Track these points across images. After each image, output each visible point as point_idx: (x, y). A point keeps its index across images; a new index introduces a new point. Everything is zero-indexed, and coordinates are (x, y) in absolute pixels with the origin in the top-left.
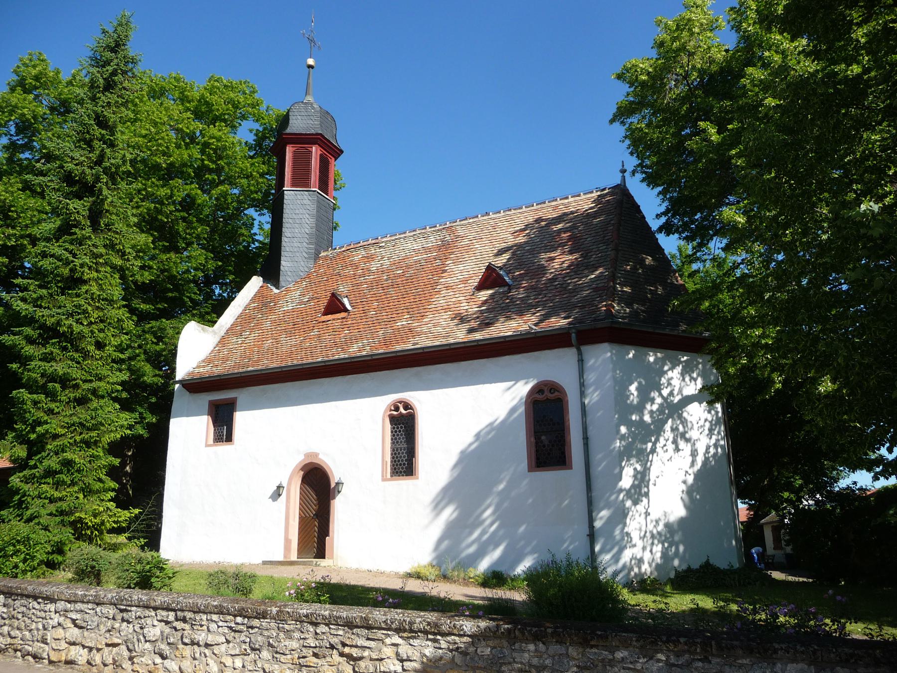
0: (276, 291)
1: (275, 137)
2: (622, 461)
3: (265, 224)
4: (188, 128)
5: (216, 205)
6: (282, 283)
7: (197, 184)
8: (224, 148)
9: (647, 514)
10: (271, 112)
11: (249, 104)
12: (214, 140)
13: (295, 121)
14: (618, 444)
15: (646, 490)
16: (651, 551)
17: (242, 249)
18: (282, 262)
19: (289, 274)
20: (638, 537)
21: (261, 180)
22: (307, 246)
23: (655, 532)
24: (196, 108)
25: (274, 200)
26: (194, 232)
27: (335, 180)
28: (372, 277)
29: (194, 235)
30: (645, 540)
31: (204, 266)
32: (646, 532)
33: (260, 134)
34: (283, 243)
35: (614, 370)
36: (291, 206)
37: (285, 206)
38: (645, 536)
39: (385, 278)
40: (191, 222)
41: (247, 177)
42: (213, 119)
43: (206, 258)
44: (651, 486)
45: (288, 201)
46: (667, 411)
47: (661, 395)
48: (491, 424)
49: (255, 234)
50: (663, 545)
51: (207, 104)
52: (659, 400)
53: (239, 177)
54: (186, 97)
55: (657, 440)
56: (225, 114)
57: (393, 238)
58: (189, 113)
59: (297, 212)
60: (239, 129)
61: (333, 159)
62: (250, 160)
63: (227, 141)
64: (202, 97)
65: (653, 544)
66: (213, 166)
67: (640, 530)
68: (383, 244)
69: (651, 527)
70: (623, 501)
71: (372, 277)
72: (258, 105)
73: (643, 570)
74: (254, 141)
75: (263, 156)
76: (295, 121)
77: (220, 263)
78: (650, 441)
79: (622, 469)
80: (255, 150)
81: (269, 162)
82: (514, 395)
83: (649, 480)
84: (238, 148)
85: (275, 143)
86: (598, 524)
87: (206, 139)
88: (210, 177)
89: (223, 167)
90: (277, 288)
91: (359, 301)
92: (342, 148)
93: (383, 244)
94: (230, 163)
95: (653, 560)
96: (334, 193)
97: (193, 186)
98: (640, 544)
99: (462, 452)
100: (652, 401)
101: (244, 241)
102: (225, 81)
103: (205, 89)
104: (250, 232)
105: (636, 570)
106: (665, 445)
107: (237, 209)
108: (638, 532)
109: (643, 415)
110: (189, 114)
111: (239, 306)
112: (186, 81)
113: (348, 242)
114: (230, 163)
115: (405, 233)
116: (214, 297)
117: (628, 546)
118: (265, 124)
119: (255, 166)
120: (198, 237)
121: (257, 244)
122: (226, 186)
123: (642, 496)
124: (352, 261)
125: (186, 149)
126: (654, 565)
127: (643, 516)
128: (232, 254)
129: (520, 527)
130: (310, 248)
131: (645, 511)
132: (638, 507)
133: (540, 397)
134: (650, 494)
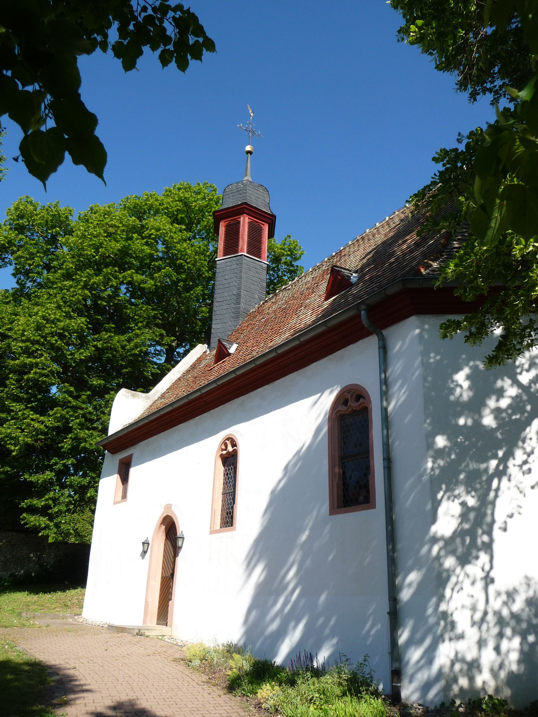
2: (438, 492)
9: (488, 580)
14: (430, 465)
15: (486, 538)
16: (497, 649)
20: (469, 622)
23: (505, 612)
30: (484, 627)
32: (486, 613)
35: (425, 354)
38: (483, 619)
44: (497, 533)
46: (529, 408)
47: (516, 382)
48: (299, 452)
50: (524, 638)
52: (512, 391)
55: (509, 454)
59: (227, 277)
65: (501, 635)
67: (474, 609)
69: (496, 604)
70: (438, 557)
73: (479, 681)
78: (495, 456)
79: (437, 504)
82: (318, 412)
83: (493, 521)
86: (405, 595)
95: (501, 666)
98: (473, 634)
99: (273, 492)
100: (500, 393)
105: (463, 682)
106: (525, 462)
108: (468, 613)
109: (481, 417)
117: (447, 636)
123: (479, 550)
126: (503, 674)
127: (480, 584)
129: (320, 595)
131: (483, 575)
132: (469, 568)
133: (342, 408)
134: (495, 546)
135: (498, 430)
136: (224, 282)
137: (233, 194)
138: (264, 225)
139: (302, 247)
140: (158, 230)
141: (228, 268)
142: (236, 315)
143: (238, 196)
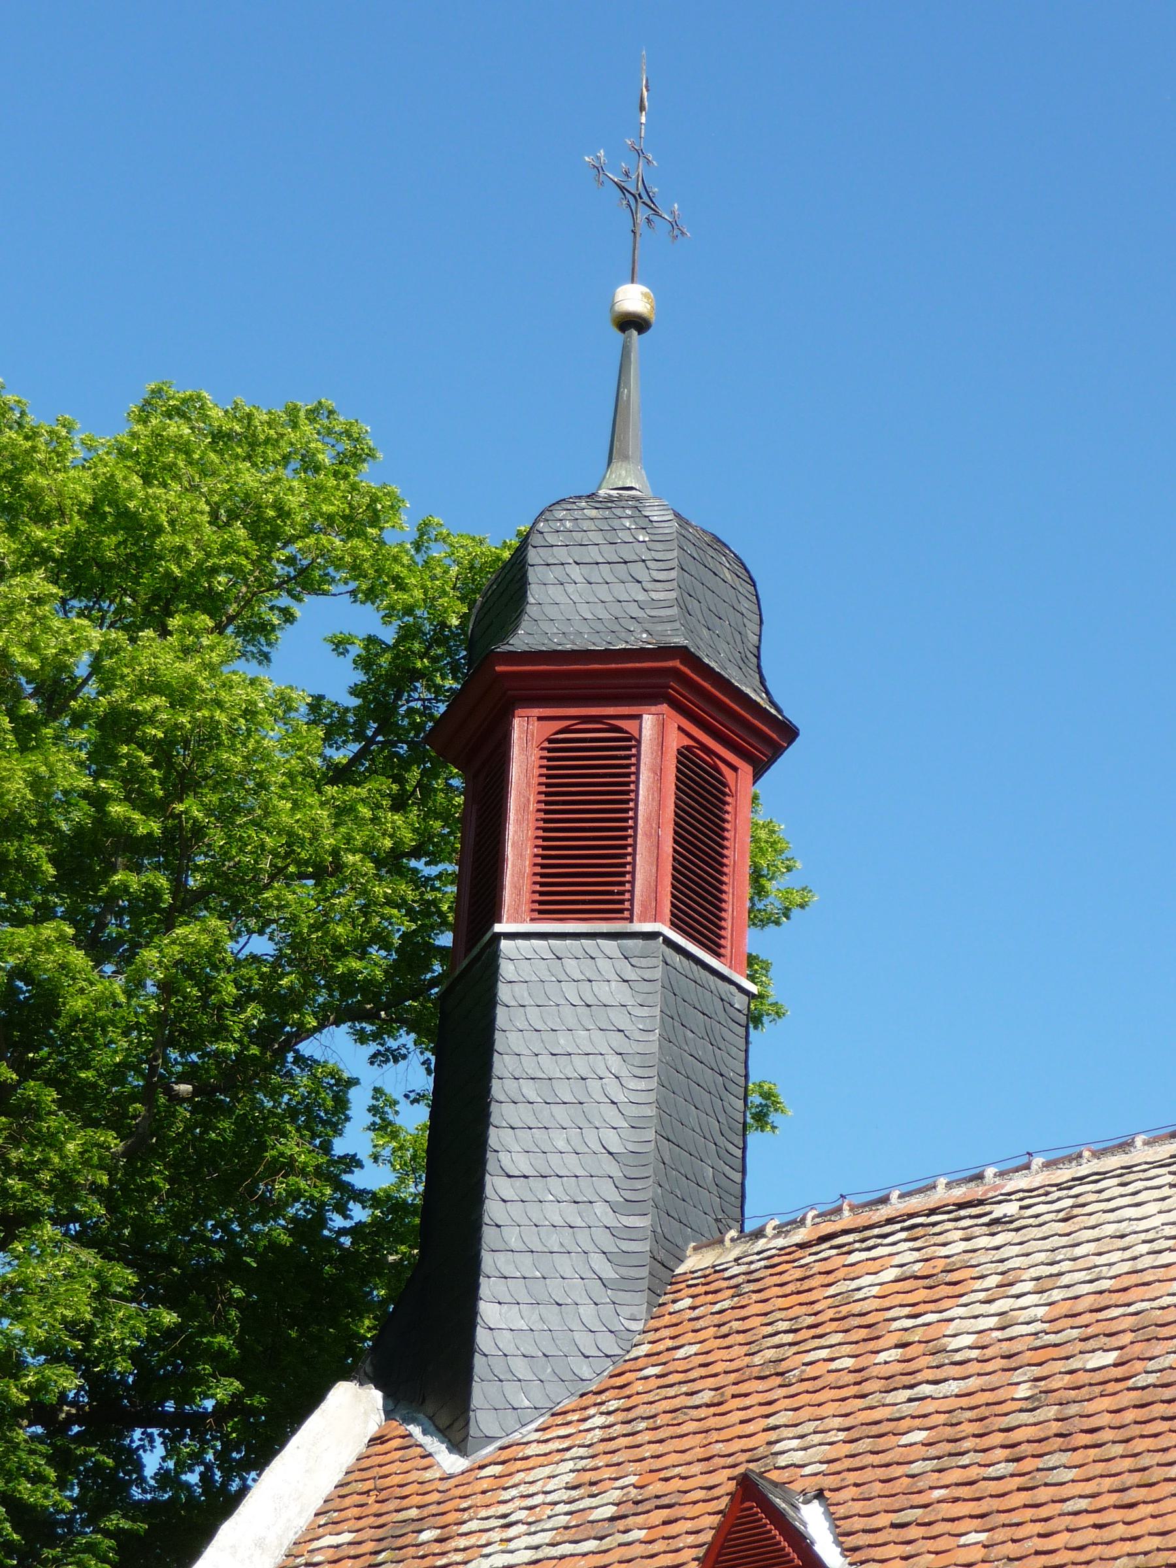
0: (449, 1462)
1: (455, 670)
3: (404, 1106)
4: (32, 647)
5: (159, 1020)
6: (483, 1419)
7: (69, 917)
8: (209, 736)
10: (438, 552)
11: (330, 519)
12: (157, 700)
13: (555, 592)
17: (285, 1239)
18: (487, 1311)
19: (521, 1368)
21: (380, 890)
22: (610, 1219)
24: (77, 545)
25: (453, 985)
26: (45, 1162)
27: (757, 875)
28: (953, 1387)
29: (46, 1176)
31: (86, 1333)
33: (385, 660)
34: (493, 1209)
36: (533, 1013)
37: (502, 1017)
39: (1023, 1391)
40: (33, 1111)
41: (320, 874)
42: (155, 598)
43: (103, 1292)
45: (520, 990)
49: (352, 1162)
51: (128, 522)
53: (277, 873)
54: (29, 497)
56: (214, 571)
57: (1064, 1174)
58: (39, 574)
59: (564, 1042)
60: (285, 637)
61: (746, 769)
62: (331, 790)
63: (219, 704)
64: (107, 491)
66: (148, 826)
68: (1011, 1208)
71: (953, 1387)
72: (375, 521)
74: (355, 691)
75: (396, 770)
76: (555, 592)
77: (169, 1318)
80: (359, 736)
81: (426, 790)
84: (272, 735)
85: (456, 699)
87: (120, 694)
88: (134, 882)
89: (199, 831)
90: (458, 1445)
91: (883, 1520)
92: (792, 714)
93: (1011, 1208)
94: (237, 810)
96: (754, 940)
97: (48, 930)
101: (295, 1195)
102: (216, 413)
103: (123, 453)
104: (326, 1148)
107: (264, 1035)
110: (38, 581)
111: (260, 1544)
112: (30, 419)
113: (828, 1199)
114: (237, 810)
115: (1125, 1146)
116: (136, 1493)
118: (409, 610)
119: (359, 821)
120: (65, 1187)
121: (360, 1213)
122: (214, 922)
124: (846, 1298)
125: (24, 749)
128: (233, 1269)
130: (630, 1233)
135: (222, 1484)
136: (549, 1066)
137: (594, 574)
138: (735, 769)
139: (799, 865)
140: (181, 696)
141: (570, 991)
142: (625, 1272)
143: (620, 592)
